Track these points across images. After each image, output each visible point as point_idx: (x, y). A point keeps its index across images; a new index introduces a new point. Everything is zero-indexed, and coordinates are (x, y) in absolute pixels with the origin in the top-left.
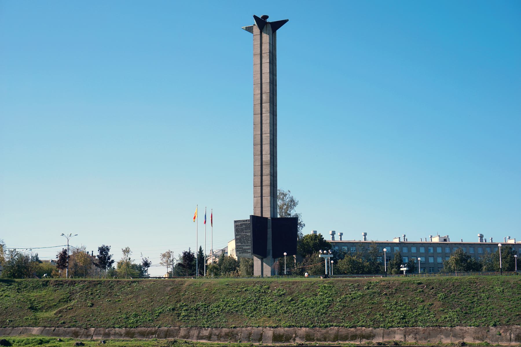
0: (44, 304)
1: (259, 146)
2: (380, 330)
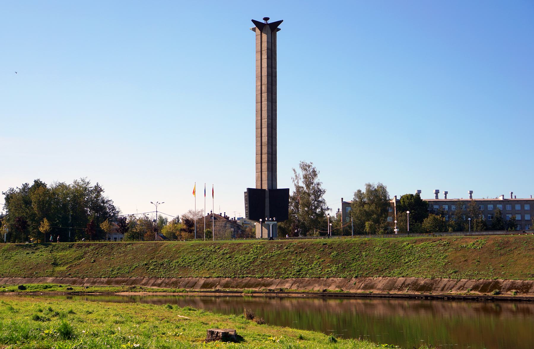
0: (63, 261)
1: (260, 130)
2: (278, 281)
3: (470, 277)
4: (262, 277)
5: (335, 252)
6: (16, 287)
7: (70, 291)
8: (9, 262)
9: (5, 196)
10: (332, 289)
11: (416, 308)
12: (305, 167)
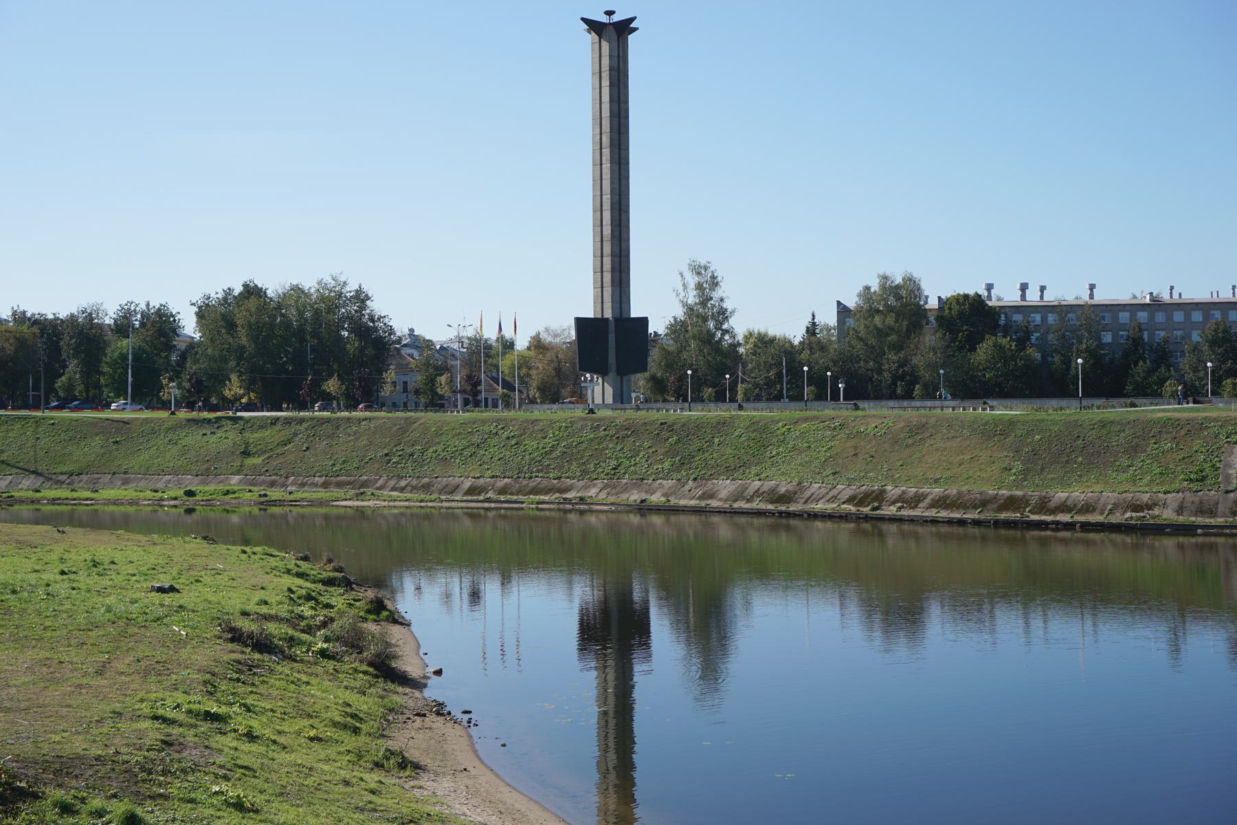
2: (581, 483)
3: (850, 482)
4: (560, 478)
5: (675, 438)
6: (180, 493)
7: (263, 499)
8: (175, 450)
9: (195, 309)
10: (656, 498)
11: (775, 528)
12: (698, 270)
